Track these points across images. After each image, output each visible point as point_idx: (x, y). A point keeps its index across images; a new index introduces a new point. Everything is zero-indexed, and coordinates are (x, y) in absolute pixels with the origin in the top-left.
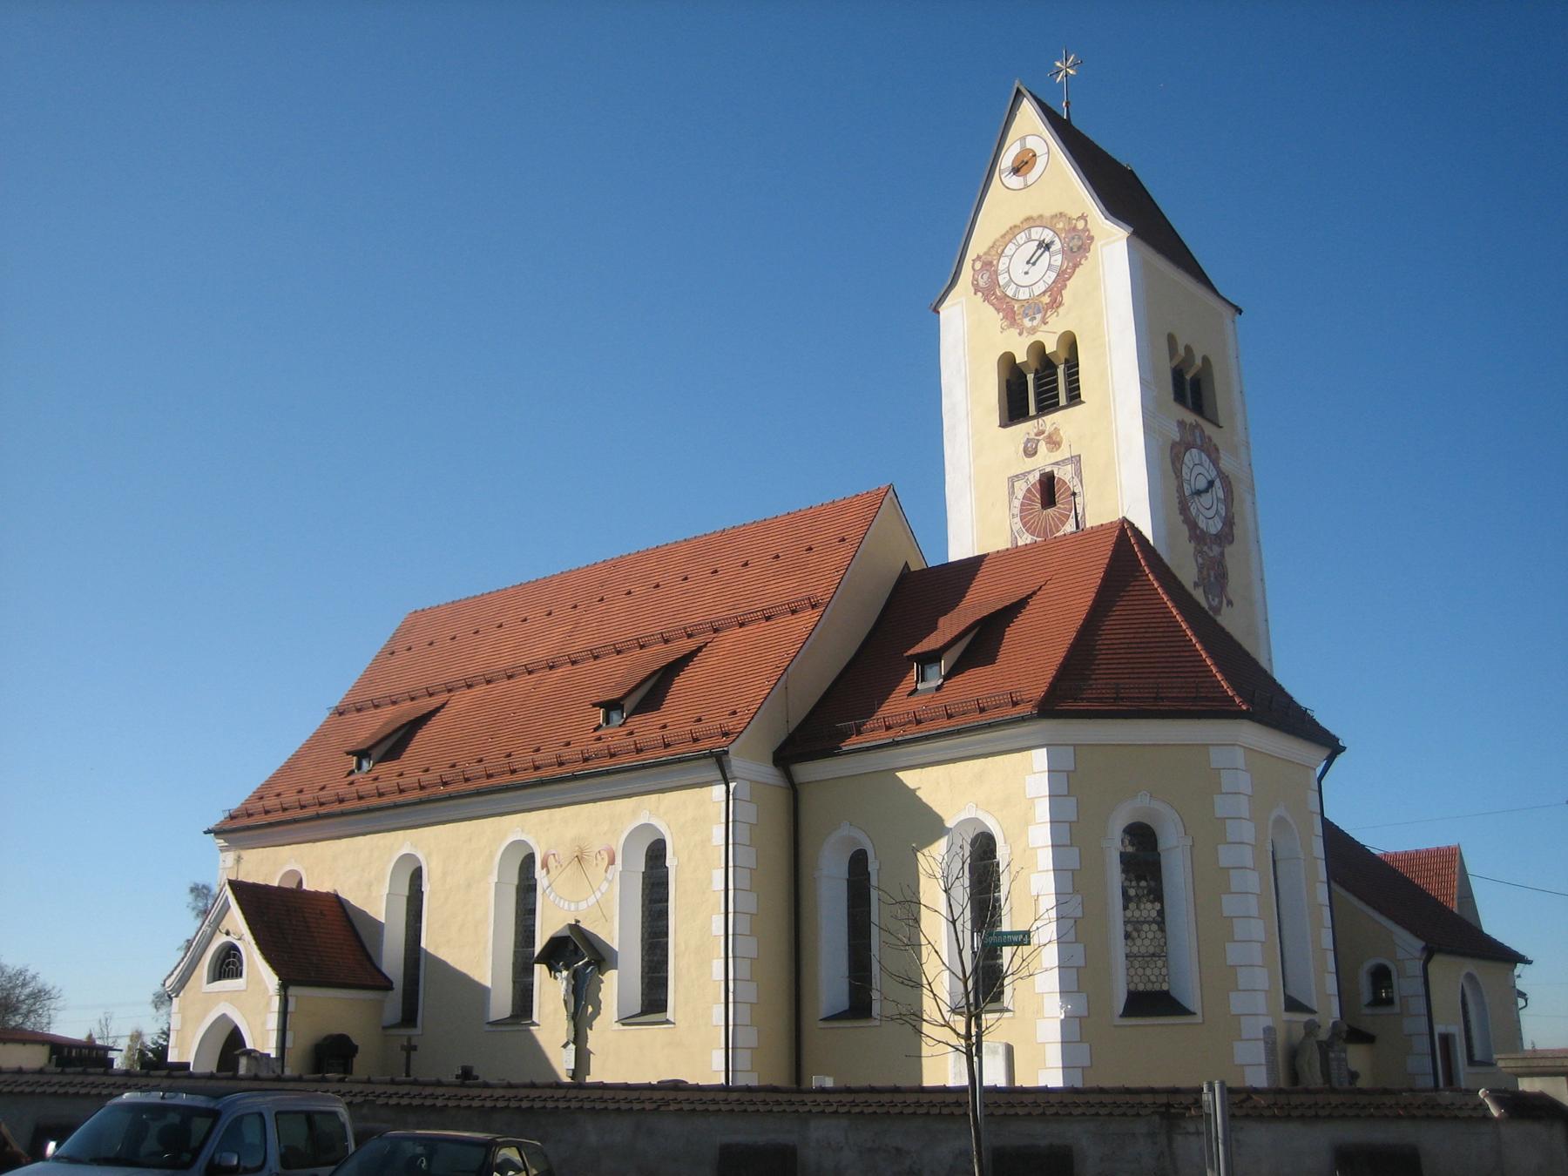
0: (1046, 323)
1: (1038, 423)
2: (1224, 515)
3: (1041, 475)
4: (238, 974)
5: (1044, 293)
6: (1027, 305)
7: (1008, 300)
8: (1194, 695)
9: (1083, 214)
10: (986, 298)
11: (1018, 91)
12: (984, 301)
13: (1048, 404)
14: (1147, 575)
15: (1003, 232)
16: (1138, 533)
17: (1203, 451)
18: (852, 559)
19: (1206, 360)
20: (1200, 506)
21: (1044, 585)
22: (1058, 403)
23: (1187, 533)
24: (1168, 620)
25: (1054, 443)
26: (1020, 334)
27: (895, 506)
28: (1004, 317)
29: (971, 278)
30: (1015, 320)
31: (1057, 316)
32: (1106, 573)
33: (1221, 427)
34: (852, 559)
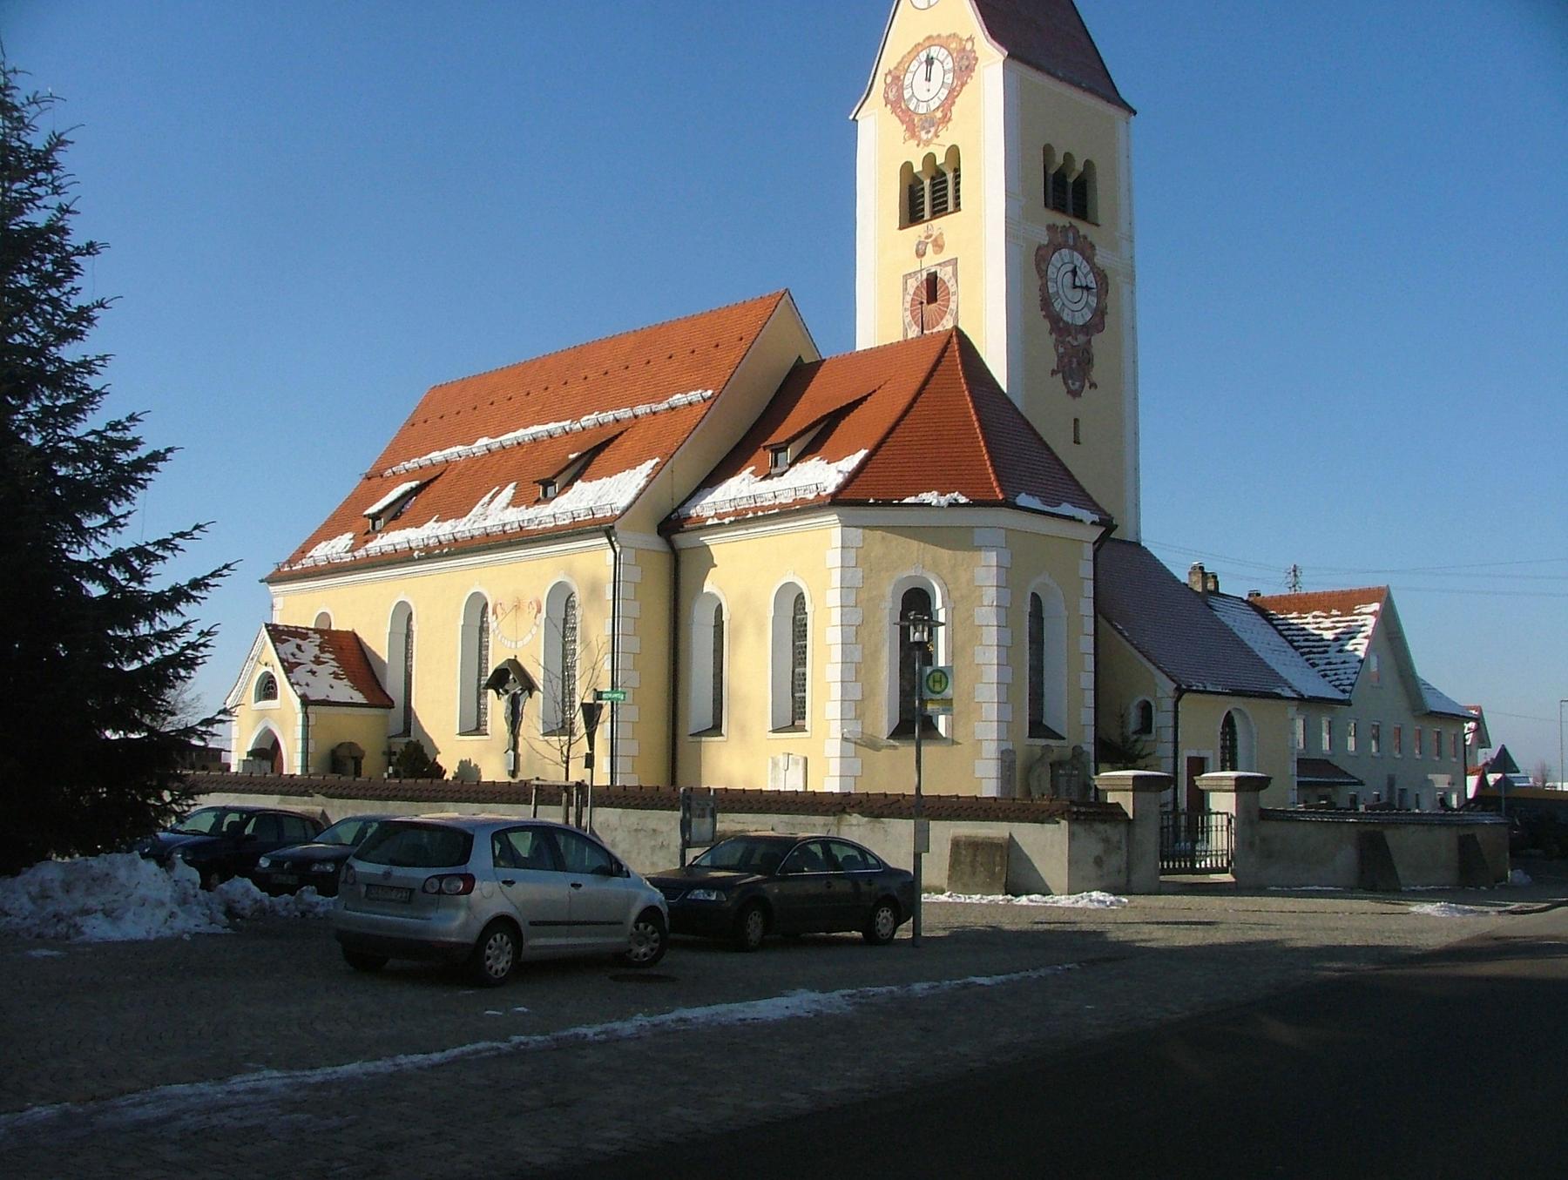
3: (928, 274)
4: (275, 697)
13: (939, 210)
15: (909, 49)
17: (1076, 250)
19: (1088, 164)
22: (946, 208)
25: (939, 246)
29: (883, 92)
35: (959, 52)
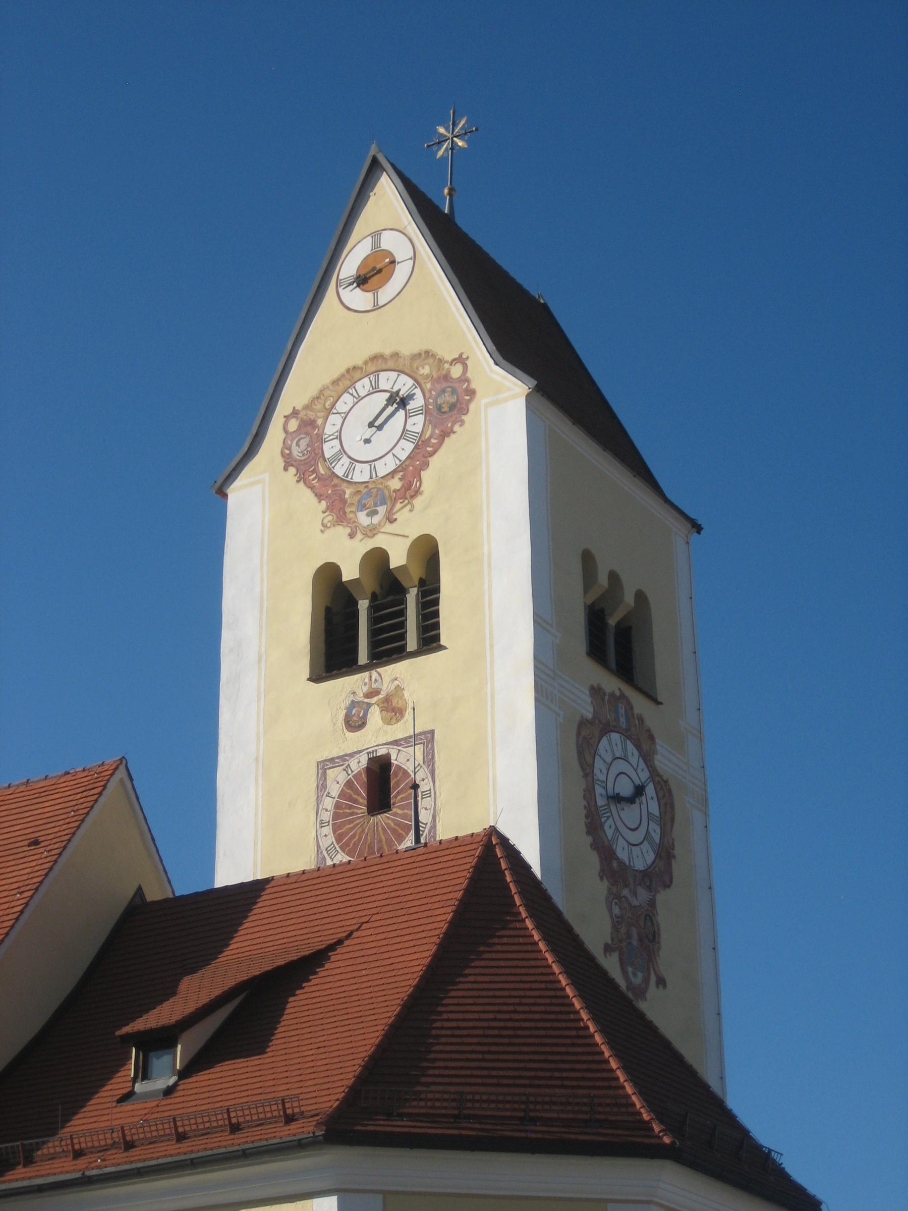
0: (392, 521)
1: (371, 677)
2: (657, 841)
5: (393, 474)
6: (364, 491)
7: (336, 481)
8: (586, 1117)
9: (461, 355)
10: (302, 478)
11: (375, 162)
12: (298, 481)
14: (523, 921)
15: (335, 376)
16: (513, 854)
18: (46, 875)
19: (640, 596)
20: (619, 824)
21: (357, 930)
22: (403, 648)
23: (597, 866)
24: (552, 993)
26: (352, 536)
27: (129, 798)
28: (328, 508)
29: (281, 445)
30: (345, 513)
31: (411, 511)
32: (457, 913)
33: (661, 703)
34: (46, 875)
35: (435, 381)
